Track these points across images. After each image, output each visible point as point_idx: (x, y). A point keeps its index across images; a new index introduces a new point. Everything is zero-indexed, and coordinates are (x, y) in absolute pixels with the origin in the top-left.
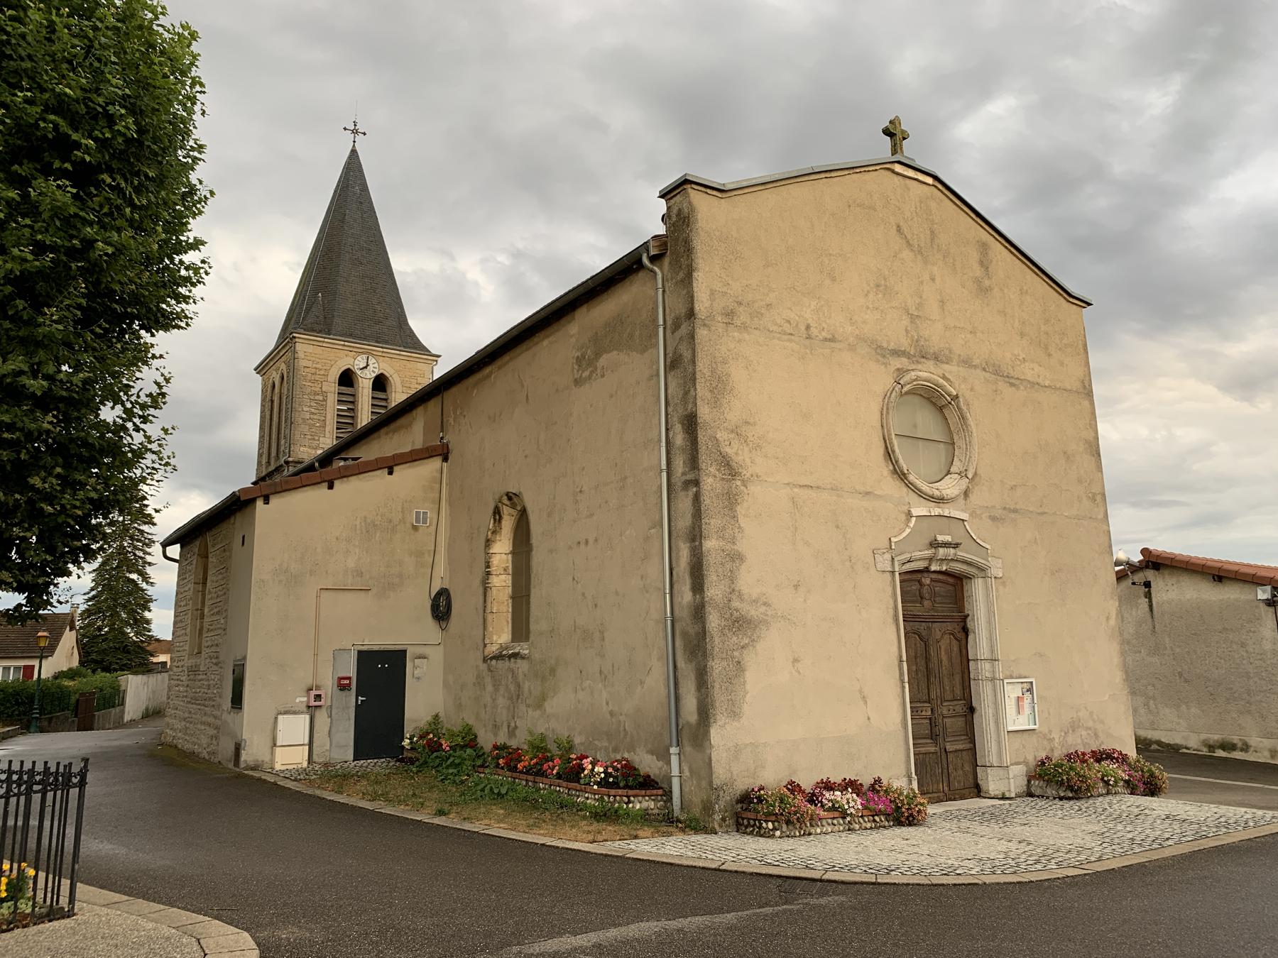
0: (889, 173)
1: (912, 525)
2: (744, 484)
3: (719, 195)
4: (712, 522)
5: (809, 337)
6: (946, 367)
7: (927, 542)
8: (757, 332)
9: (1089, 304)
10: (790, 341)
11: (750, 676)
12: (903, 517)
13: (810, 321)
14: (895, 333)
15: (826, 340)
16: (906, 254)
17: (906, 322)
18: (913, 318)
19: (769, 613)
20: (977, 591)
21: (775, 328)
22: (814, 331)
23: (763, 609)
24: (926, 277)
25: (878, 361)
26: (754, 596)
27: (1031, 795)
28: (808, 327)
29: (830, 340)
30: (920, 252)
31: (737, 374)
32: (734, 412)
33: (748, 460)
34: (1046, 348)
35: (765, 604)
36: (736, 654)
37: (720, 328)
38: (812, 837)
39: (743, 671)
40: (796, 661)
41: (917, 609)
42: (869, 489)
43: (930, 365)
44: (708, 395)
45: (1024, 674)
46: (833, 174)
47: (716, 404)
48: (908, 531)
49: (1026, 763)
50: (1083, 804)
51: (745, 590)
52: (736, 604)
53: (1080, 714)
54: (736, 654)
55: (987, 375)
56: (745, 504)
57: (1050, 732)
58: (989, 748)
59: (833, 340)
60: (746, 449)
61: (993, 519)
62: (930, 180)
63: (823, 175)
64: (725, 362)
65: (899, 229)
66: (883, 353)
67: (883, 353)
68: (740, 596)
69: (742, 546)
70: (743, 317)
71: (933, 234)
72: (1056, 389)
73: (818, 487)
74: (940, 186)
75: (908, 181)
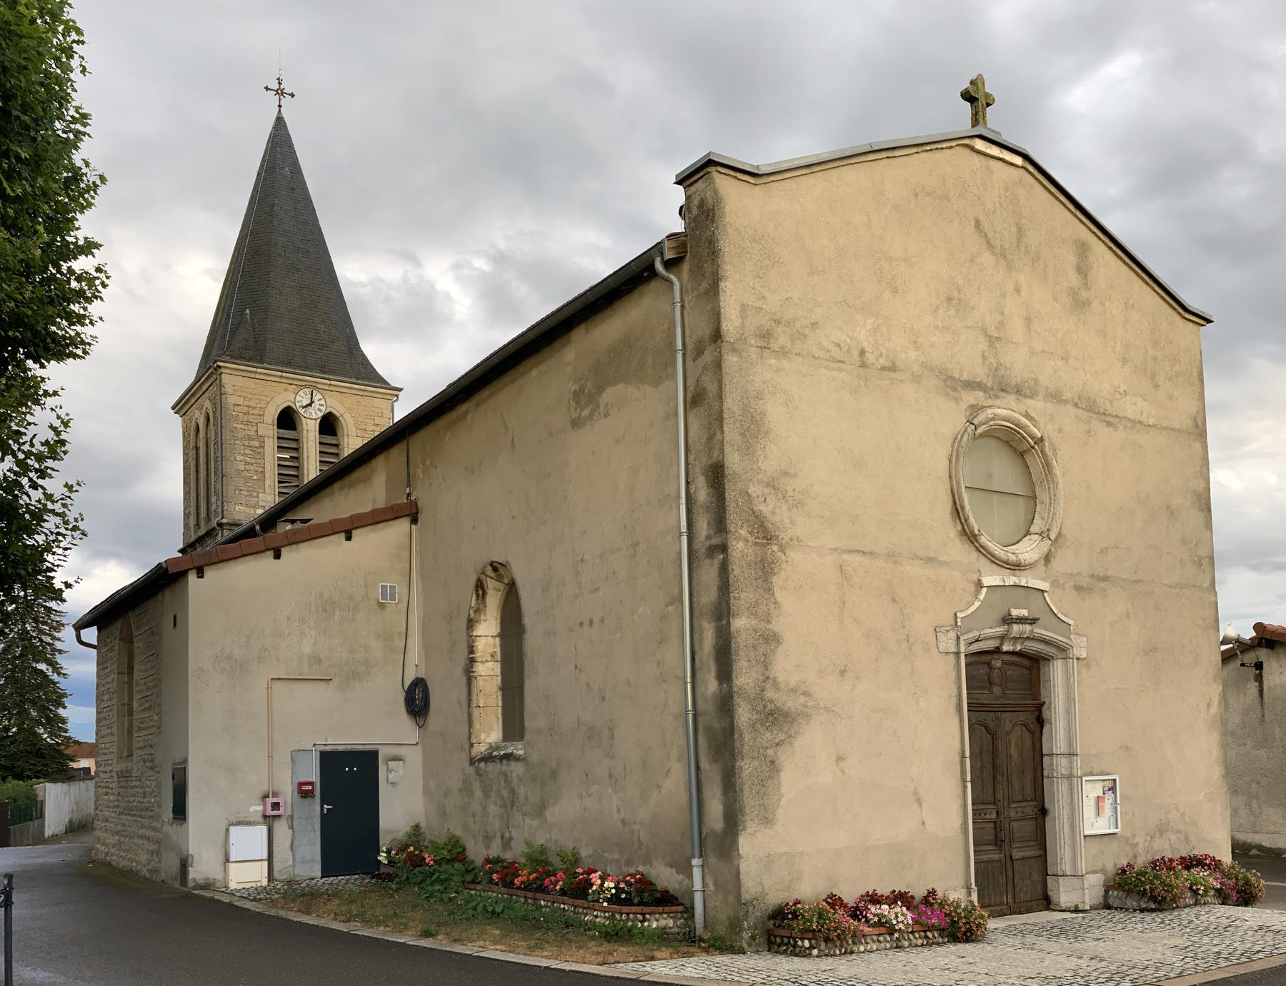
0: (967, 151)
1: (981, 597)
4: (743, 595)
6: (1030, 402)
10: (840, 370)
12: (972, 588)
13: (865, 345)
16: (987, 258)
17: (983, 345)
19: (810, 704)
22: (870, 358)
23: (802, 699)
26: (793, 684)
27: (1108, 907)
28: (862, 352)
30: (1004, 256)
31: (774, 412)
32: (770, 460)
33: (787, 521)
35: (805, 694)
36: (770, 752)
37: (753, 353)
38: (854, 956)
39: (778, 771)
41: (985, 697)
42: (932, 555)
43: (1010, 400)
44: (739, 439)
46: (897, 153)
47: (748, 451)
48: (977, 604)
49: (1103, 871)
51: (781, 678)
52: (770, 694)
53: (1170, 816)
54: (770, 752)
56: (783, 574)
57: (1134, 836)
58: (1062, 854)
59: (892, 368)
61: (1079, 588)
62: (1018, 160)
64: (759, 397)
65: (978, 224)
66: (954, 385)
67: (954, 385)
69: (777, 625)
73: (871, 553)
74: (1031, 168)
75: (992, 162)
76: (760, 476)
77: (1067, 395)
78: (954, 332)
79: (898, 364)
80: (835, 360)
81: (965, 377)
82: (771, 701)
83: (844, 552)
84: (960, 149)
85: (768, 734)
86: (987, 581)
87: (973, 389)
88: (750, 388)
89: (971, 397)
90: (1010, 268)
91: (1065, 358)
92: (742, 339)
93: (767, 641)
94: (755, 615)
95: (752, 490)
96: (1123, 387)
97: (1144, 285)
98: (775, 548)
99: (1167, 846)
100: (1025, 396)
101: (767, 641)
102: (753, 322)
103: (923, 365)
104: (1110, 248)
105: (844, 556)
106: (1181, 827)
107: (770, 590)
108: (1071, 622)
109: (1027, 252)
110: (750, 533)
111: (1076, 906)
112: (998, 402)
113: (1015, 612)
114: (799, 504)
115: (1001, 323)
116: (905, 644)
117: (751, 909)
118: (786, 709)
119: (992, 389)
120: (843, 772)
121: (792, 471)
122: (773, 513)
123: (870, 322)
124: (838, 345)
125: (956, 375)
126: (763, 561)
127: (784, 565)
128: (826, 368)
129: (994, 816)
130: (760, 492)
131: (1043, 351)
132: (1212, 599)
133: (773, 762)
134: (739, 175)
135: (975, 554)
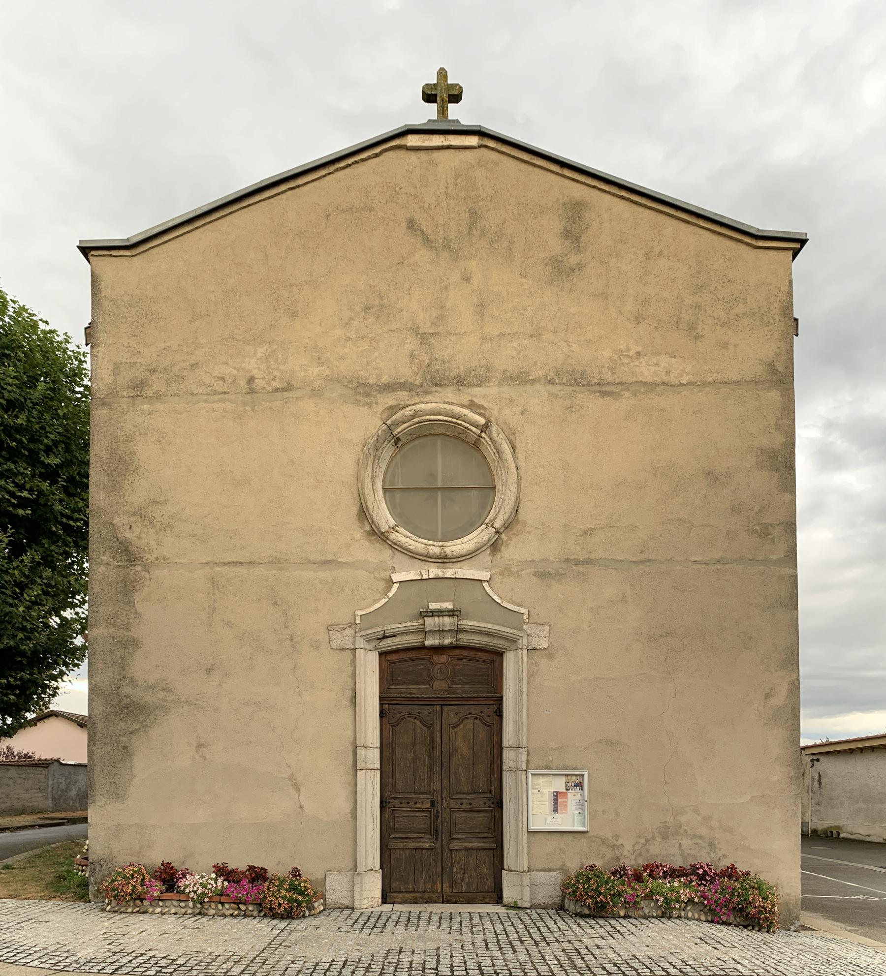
0: (401, 153)
1: (390, 594)
2: (146, 569)
3: (127, 253)
4: (101, 609)
5: (252, 391)
6: (477, 391)
7: (416, 612)
8: (176, 399)
9: (796, 244)
10: (222, 401)
11: (139, 761)
12: (382, 585)
13: (255, 372)
14: (393, 358)
15: (277, 390)
16: (423, 256)
17: (412, 344)
18: (424, 338)
19: (170, 698)
20: (513, 668)
21: (201, 390)
22: (259, 383)
23: (161, 695)
24: (455, 277)
25: (357, 402)
26: (151, 681)
27: (561, 908)
28: (251, 380)
29: (283, 390)
30: (447, 247)
31: (146, 451)
32: (138, 492)
33: (153, 544)
34: (692, 327)
35: (163, 690)
36: (123, 739)
37: (125, 403)
38: (146, 916)
39: (130, 756)
40: (200, 746)
41: (396, 691)
42: (330, 557)
43: (449, 394)
44: (105, 479)
45: (579, 766)
46: (300, 181)
47: (115, 487)
48: (384, 601)
49: (562, 869)
50: (757, 936)
51: (139, 676)
52: (126, 690)
53: (683, 819)
54: (123, 739)
55: (555, 389)
56: (146, 590)
57: (617, 837)
58: (515, 851)
59: (289, 388)
60: (152, 531)
61: (542, 575)
62: (473, 141)
63: (283, 187)
64: (129, 439)
65: (412, 225)
66: (363, 390)
67: (363, 390)
68: (133, 683)
69: (137, 632)
70: (157, 384)
71: (474, 215)
72: (704, 384)
73: (251, 563)
74: (492, 144)
75: (436, 154)
76: (126, 508)
77: (538, 373)
78: (372, 339)
79: (294, 383)
80: (216, 393)
81: (385, 379)
82: (127, 697)
83: (217, 564)
84: (391, 154)
85: (122, 724)
86: (396, 577)
87: (394, 390)
88: (119, 433)
89: (390, 400)
90: (456, 257)
91: (536, 335)
92: (113, 393)
93: (125, 647)
94: (114, 625)
95: (116, 520)
96: (635, 349)
97: (683, 226)
98: (139, 568)
99: (675, 850)
100: (470, 385)
101: (125, 647)
102: (126, 376)
103: (328, 379)
104: (622, 197)
105: (218, 569)
106: (703, 831)
107: (130, 603)
108: (522, 610)
109: (483, 234)
110: (113, 558)
111: (515, 902)
112: (429, 398)
113: (433, 606)
114: (167, 527)
115: (441, 318)
116: (288, 642)
117: (98, 868)
118: (142, 703)
119: (421, 386)
120: (204, 758)
121: (162, 499)
122: (139, 537)
123: (261, 351)
124: (223, 379)
125: (372, 381)
126: (124, 581)
127: (147, 583)
128: (206, 401)
129: (428, 805)
130: (125, 522)
131: (501, 335)
132: (787, 571)
133: (125, 747)
134: (114, 253)
135: (390, 552)
